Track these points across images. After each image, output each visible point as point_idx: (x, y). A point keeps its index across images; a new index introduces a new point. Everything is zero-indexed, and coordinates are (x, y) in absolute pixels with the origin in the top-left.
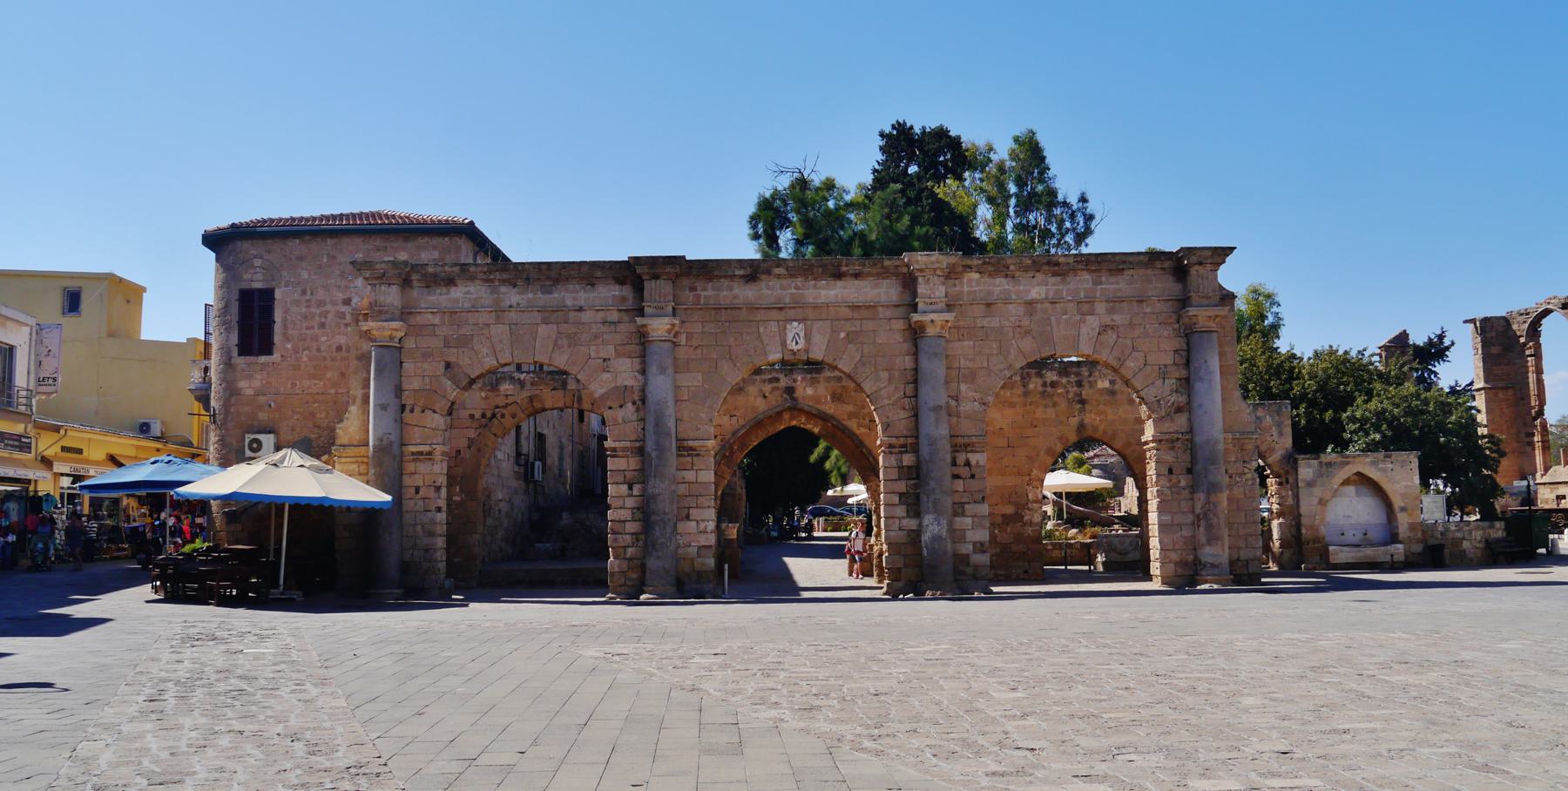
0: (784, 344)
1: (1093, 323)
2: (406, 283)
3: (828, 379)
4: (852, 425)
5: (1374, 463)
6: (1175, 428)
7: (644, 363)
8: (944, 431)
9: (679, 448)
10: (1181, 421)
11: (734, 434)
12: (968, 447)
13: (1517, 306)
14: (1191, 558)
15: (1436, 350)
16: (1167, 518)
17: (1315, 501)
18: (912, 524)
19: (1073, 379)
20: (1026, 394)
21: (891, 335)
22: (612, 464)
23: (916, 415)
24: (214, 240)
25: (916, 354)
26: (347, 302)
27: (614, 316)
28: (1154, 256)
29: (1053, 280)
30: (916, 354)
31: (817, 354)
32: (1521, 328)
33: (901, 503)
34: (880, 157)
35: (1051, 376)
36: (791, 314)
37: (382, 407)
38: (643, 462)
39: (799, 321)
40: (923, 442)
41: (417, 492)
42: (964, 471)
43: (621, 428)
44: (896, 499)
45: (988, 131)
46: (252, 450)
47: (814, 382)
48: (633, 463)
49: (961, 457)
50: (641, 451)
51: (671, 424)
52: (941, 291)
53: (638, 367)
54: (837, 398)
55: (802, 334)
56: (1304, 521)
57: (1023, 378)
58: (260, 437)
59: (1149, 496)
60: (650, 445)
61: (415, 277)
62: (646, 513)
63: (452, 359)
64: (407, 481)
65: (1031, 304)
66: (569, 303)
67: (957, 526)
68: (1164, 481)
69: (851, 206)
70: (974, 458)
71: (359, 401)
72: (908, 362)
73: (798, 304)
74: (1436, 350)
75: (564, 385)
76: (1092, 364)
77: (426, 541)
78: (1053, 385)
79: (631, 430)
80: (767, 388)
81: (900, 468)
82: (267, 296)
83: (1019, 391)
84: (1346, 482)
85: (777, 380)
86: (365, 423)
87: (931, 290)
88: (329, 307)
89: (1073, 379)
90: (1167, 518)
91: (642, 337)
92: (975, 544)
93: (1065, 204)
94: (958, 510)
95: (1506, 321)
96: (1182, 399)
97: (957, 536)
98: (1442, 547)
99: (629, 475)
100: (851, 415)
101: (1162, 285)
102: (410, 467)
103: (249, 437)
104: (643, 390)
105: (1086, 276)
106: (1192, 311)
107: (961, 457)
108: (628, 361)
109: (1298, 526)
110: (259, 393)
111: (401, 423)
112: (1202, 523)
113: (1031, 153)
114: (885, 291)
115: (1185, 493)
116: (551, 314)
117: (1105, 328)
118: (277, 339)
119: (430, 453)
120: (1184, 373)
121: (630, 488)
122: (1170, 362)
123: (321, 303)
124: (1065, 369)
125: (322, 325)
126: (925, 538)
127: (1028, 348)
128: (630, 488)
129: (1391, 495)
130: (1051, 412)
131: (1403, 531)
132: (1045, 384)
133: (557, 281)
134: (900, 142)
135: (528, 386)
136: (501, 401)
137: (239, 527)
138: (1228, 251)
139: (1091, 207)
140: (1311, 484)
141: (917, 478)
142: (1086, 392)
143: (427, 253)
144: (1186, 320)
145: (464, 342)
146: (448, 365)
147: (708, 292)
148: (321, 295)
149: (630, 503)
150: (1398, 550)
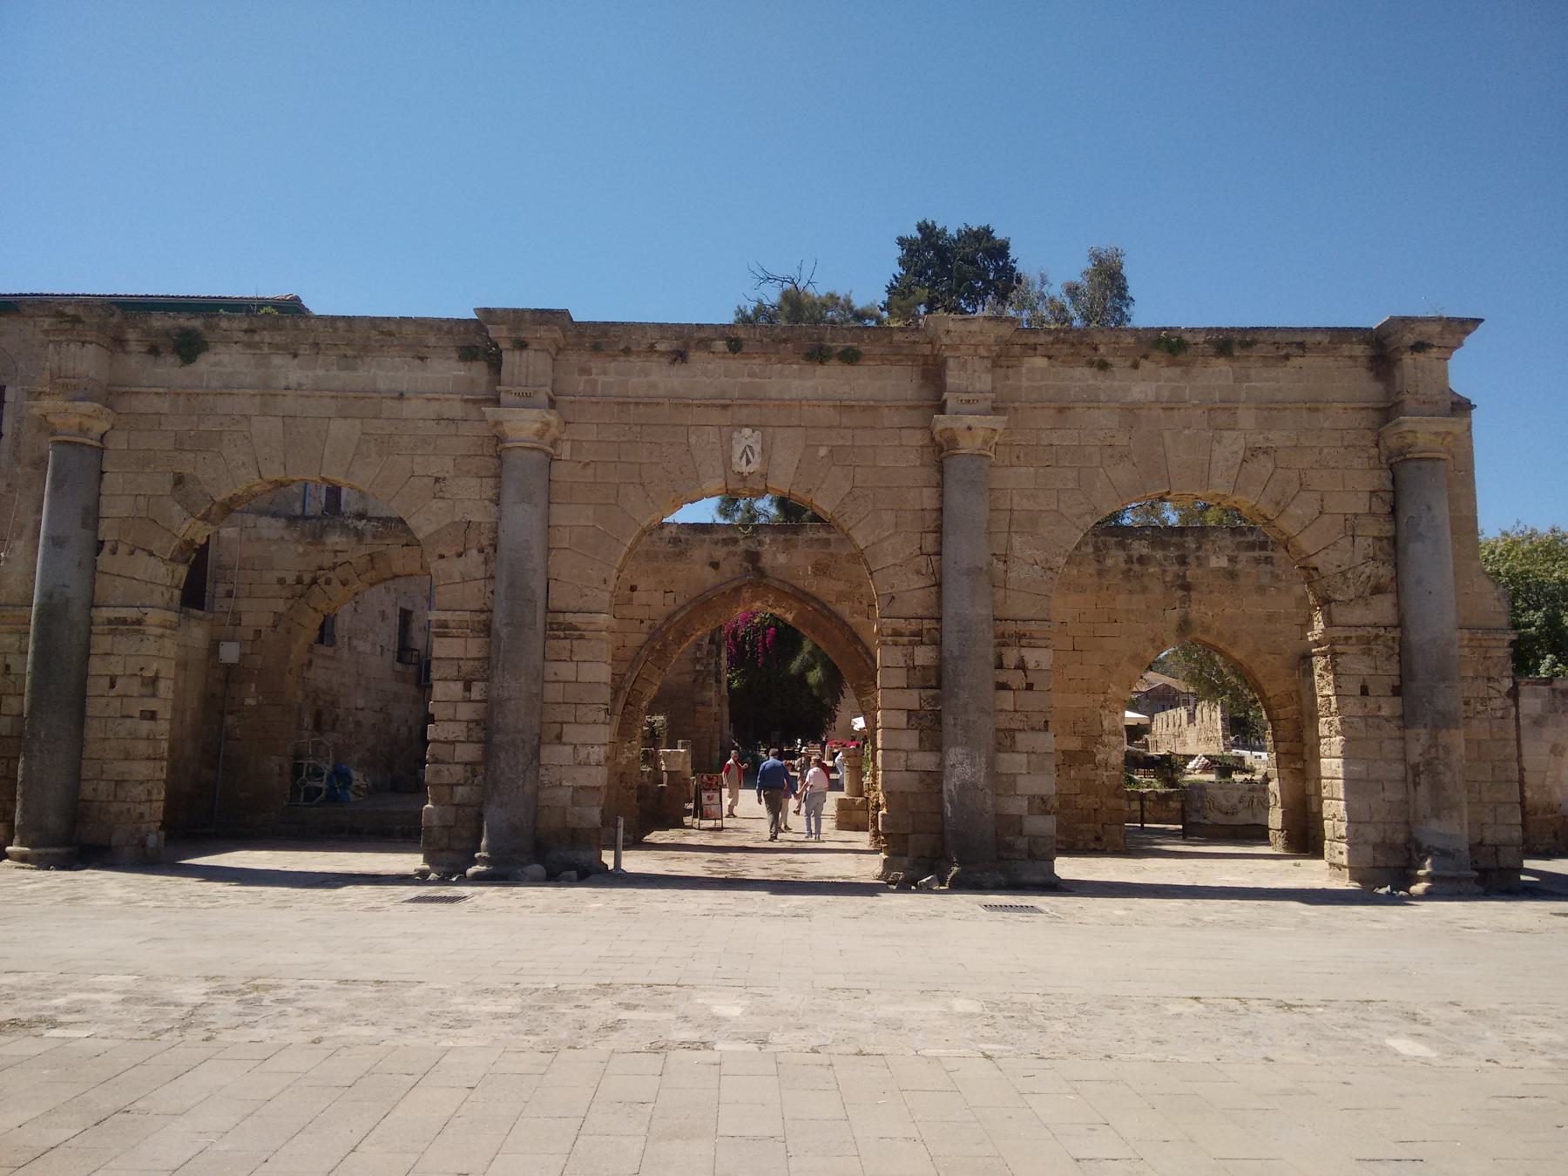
0: (727, 463)
1: (1231, 446)
4: (844, 609)
6: (1370, 618)
7: (498, 486)
9: (550, 626)
10: (1383, 609)
11: (669, 618)
14: (1400, 838)
16: (1357, 768)
17: (1546, 748)
18: (927, 761)
19: (1173, 552)
20: (1100, 573)
21: (903, 456)
23: (939, 585)
25: (941, 485)
28: (1341, 335)
30: (941, 485)
34: (898, 270)
37: (56, 542)
38: (489, 644)
39: (754, 427)
40: (949, 624)
41: (112, 686)
42: (1016, 679)
43: (457, 586)
47: (789, 546)
49: (1011, 656)
50: (487, 629)
51: (538, 585)
52: (984, 381)
53: (490, 493)
54: (821, 570)
55: (757, 448)
57: (1097, 549)
59: (1323, 730)
60: (499, 619)
62: (486, 729)
63: (187, 470)
64: (96, 665)
65: (1131, 411)
66: (382, 385)
67: (1003, 769)
68: (1353, 706)
70: (1032, 657)
72: (928, 498)
78: (1142, 560)
80: (720, 553)
83: (1092, 568)
85: (735, 541)
87: (968, 378)
89: (1173, 552)
90: (1357, 768)
94: (1005, 740)
96: (1385, 572)
97: (1001, 783)
99: (467, 667)
100: (841, 597)
101: (1352, 382)
102: (101, 643)
106: (1407, 422)
107: (1011, 656)
108: (475, 482)
112: (1423, 779)
115: (1391, 729)
119: (139, 622)
120: (1387, 529)
121: (468, 688)
124: (1161, 535)
126: (950, 785)
128: (468, 688)
132: (1129, 560)
133: (366, 349)
135: (368, 539)
136: (327, 560)
138: (1467, 325)
140: (1538, 722)
142: (1192, 573)
144: (1393, 442)
146: (179, 480)
147: (611, 376)
149: (466, 712)
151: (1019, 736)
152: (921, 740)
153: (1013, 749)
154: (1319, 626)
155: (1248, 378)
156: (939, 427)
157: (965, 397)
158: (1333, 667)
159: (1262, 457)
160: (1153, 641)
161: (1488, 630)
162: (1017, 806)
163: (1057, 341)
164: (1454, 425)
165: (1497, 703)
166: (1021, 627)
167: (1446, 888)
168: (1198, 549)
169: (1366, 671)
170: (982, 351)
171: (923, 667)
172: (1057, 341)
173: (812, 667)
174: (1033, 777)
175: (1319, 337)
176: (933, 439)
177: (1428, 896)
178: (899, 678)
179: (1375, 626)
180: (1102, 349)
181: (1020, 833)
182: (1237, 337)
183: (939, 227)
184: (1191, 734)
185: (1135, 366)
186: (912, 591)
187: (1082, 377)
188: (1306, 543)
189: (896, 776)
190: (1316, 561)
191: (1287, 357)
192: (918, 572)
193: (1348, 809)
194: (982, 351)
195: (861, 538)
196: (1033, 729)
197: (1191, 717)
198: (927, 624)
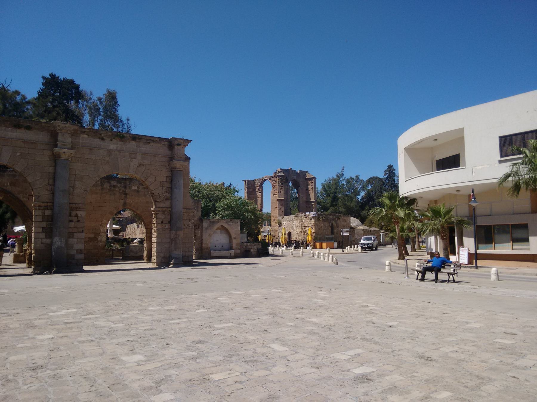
4: (21, 196)
5: (226, 222)
10: (168, 204)
12: (76, 209)
13: (257, 178)
14: (168, 255)
16: (160, 240)
18: (48, 241)
20: (102, 189)
23: (53, 193)
25: (55, 167)
28: (162, 139)
29: (120, 143)
30: (55, 167)
32: (258, 184)
33: (43, 232)
34: (42, 87)
35: (113, 183)
42: (75, 219)
44: (41, 230)
45: (94, 88)
49: (74, 213)
56: (204, 242)
57: (101, 183)
59: (153, 231)
65: (110, 152)
68: (160, 226)
69: (28, 103)
70: (80, 213)
72: (51, 170)
76: (131, 180)
78: (114, 186)
81: (44, 216)
83: (100, 188)
84: (218, 229)
87: (64, 139)
89: (122, 185)
92: (77, 250)
93: (121, 121)
94: (71, 235)
95: (254, 182)
96: (169, 195)
101: (164, 150)
106: (175, 162)
107: (74, 213)
109: (202, 244)
113: (112, 97)
114: (42, 137)
117: (140, 165)
120: (170, 185)
122: (165, 181)
126: (54, 247)
127: (105, 170)
129: (231, 234)
131: (234, 246)
132: (110, 186)
134: (53, 84)
139: (131, 122)
140: (207, 229)
141: (52, 221)
142: (127, 191)
150: (232, 252)
151: (75, 234)
152: (46, 235)
153: (73, 237)
154: (154, 207)
155: (140, 147)
156: (55, 151)
157: (63, 144)
158: (156, 217)
159: (142, 166)
160: (116, 208)
161: (189, 209)
162: (73, 252)
163: (90, 131)
164: (186, 163)
165: (191, 225)
166: (77, 206)
167: (176, 265)
168: (130, 184)
169: (162, 217)
170: (69, 132)
171: (48, 216)
172: (90, 131)
173: (7, 213)
174: (78, 244)
175: (157, 139)
176: (53, 154)
177: (172, 267)
178: (40, 219)
179: (166, 207)
180: (103, 135)
181: (74, 259)
182: (137, 137)
183: (57, 76)
184: (138, 231)
185: (111, 140)
186: (45, 195)
187: (96, 141)
188: (152, 188)
189: (38, 245)
190: (153, 192)
191: (149, 143)
192: (47, 190)
193: (157, 249)
194: (69, 132)
195: (30, 179)
196: (79, 232)
197: (138, 227)
198: (49, 204)
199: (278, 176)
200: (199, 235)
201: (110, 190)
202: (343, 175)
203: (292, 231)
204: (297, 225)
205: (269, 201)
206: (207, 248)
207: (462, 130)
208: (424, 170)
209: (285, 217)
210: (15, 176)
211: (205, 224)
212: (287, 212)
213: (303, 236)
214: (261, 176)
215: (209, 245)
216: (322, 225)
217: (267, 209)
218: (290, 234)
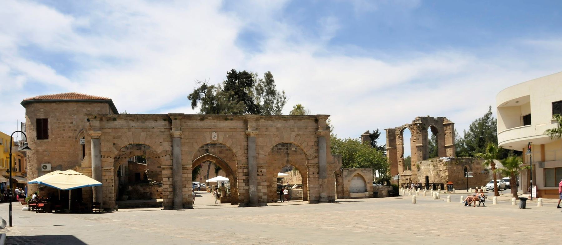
0: (211, 138)
1: (294, 134)
2: (101, 120)
3: (218, 147)
4: (225, 160)
8: (255, 163)
12: (261, 167)
15: (375, 135)
18: (247, 188)
19: (285, 147)
22: (164, 172)
24: (26, 104)
25: (247, 141)
26: (72, 123)
27: (163, 130)
29: (284, 122)
30: (247, 141)
31: (221, 141)
32: (398, 132)
36: (214, 130)
40: (250, 166)
42: (260, 174)
46: (44, 169)
47: (214, 148)
48: (169, 172)
49: (260, 170)
50: (171, 169)
52: (254, 125)
56: (345, 186)
58: (46, 165)
61: (104, 118)
63: (115, 142)
65: (278, 128)
71: (88, 154)
72: (245, 144)
73: (215, 127)
74: (375, 135)
75: (140, 148)
77: (110, 195)
78: (280, 149)
79: (169, 163)
81: (243, 173)
82: (46, 121)
86: (92, 160)
88: (66, 124)
89: (285, 147)
91: (172, 137)
94: (259, 184)
96: (316, 154)
97: (258, 190)
98: (377, 192)
99: (168, 175)
101: (312, 124)
102: (104, 174)
103: (42, 165)
104: (172, 151)
105: (292, 121)
107: (260, 170)
109: (343, 188)
110: (45, 151)
111: (101, 161)
113: (269, 77)
114: (239, 124)
116: (145, 129)
117: (297, 135)
118: (49, 134)
120: (317, 148)
122: (313, 144)
123: (63, 123)
125: (64, 130)
126: (251, 191)
127: (276, 141)
130: (279, 157)
134: (233, 75)
136: (121, 153)
137: (44, 192)
140: (346, 176)
142: (289, 151)
143: (96, 109)
145: (119, 137)
146: (114, 144)
147: (190, 123)
148: (63, 120)
149: (169, 183)
150: (367, 194)
162: (261, 194)
164: (327, 132)
186: (243, 159)
188: (305, 150)
199: (416, 124)
200: (341, 181)
201: (277, 152)
202: (491, 113)
203: (429, 175)
204: (429, 170)
205: (408, 145)
206: (347, 191)
207: (529, 96)
208: (511, 126)
209: (424, 162)
210: (221, 147)
211: (345, 173)
212: (425, 158)
213: (438, 179)
214: (400, 124)
215: (349, 189)
216: (455, 168)
217: (407, 153)
218: (427, 178)
